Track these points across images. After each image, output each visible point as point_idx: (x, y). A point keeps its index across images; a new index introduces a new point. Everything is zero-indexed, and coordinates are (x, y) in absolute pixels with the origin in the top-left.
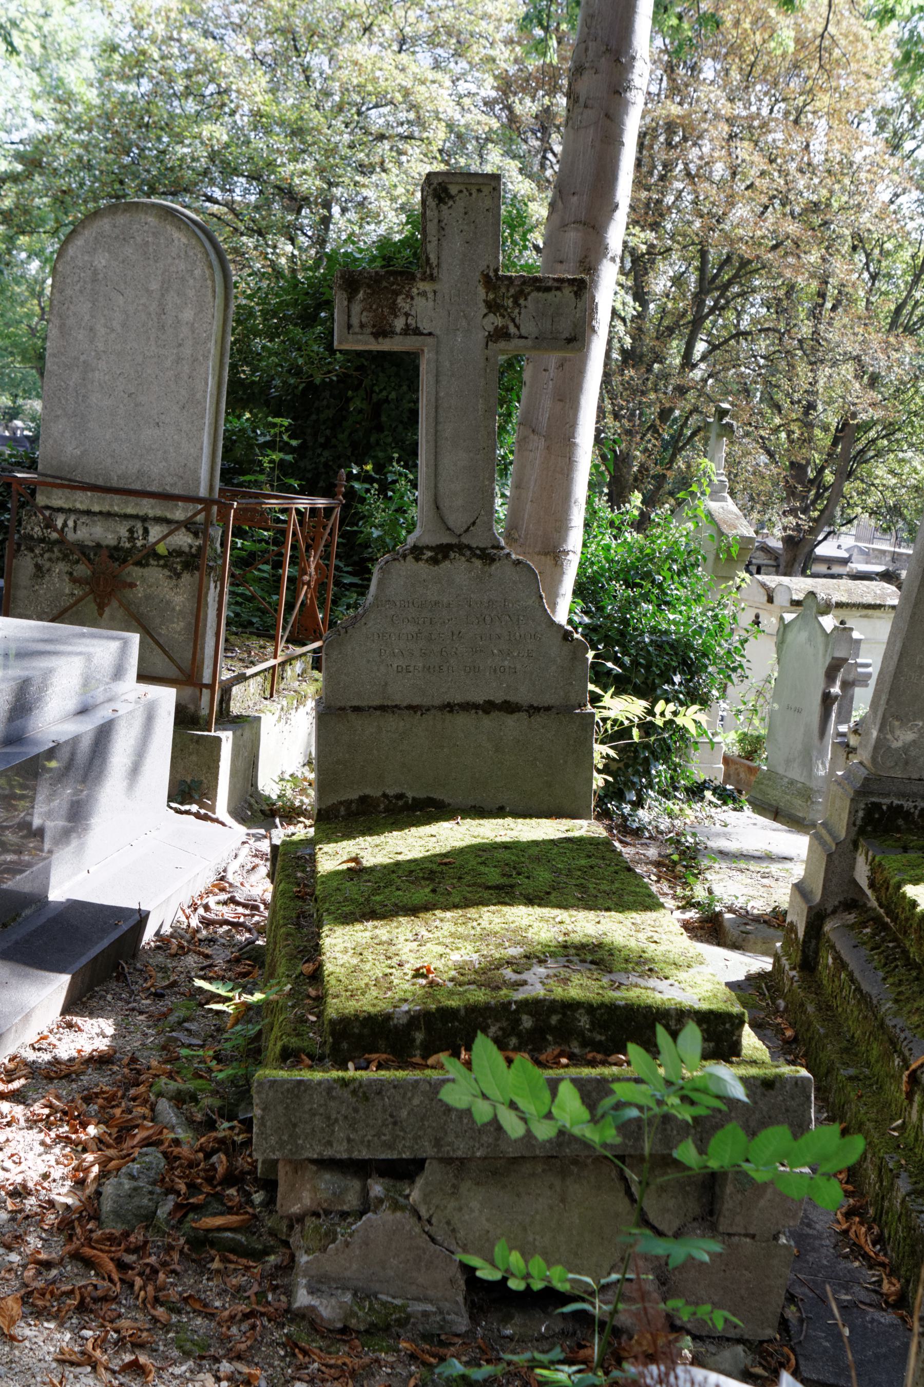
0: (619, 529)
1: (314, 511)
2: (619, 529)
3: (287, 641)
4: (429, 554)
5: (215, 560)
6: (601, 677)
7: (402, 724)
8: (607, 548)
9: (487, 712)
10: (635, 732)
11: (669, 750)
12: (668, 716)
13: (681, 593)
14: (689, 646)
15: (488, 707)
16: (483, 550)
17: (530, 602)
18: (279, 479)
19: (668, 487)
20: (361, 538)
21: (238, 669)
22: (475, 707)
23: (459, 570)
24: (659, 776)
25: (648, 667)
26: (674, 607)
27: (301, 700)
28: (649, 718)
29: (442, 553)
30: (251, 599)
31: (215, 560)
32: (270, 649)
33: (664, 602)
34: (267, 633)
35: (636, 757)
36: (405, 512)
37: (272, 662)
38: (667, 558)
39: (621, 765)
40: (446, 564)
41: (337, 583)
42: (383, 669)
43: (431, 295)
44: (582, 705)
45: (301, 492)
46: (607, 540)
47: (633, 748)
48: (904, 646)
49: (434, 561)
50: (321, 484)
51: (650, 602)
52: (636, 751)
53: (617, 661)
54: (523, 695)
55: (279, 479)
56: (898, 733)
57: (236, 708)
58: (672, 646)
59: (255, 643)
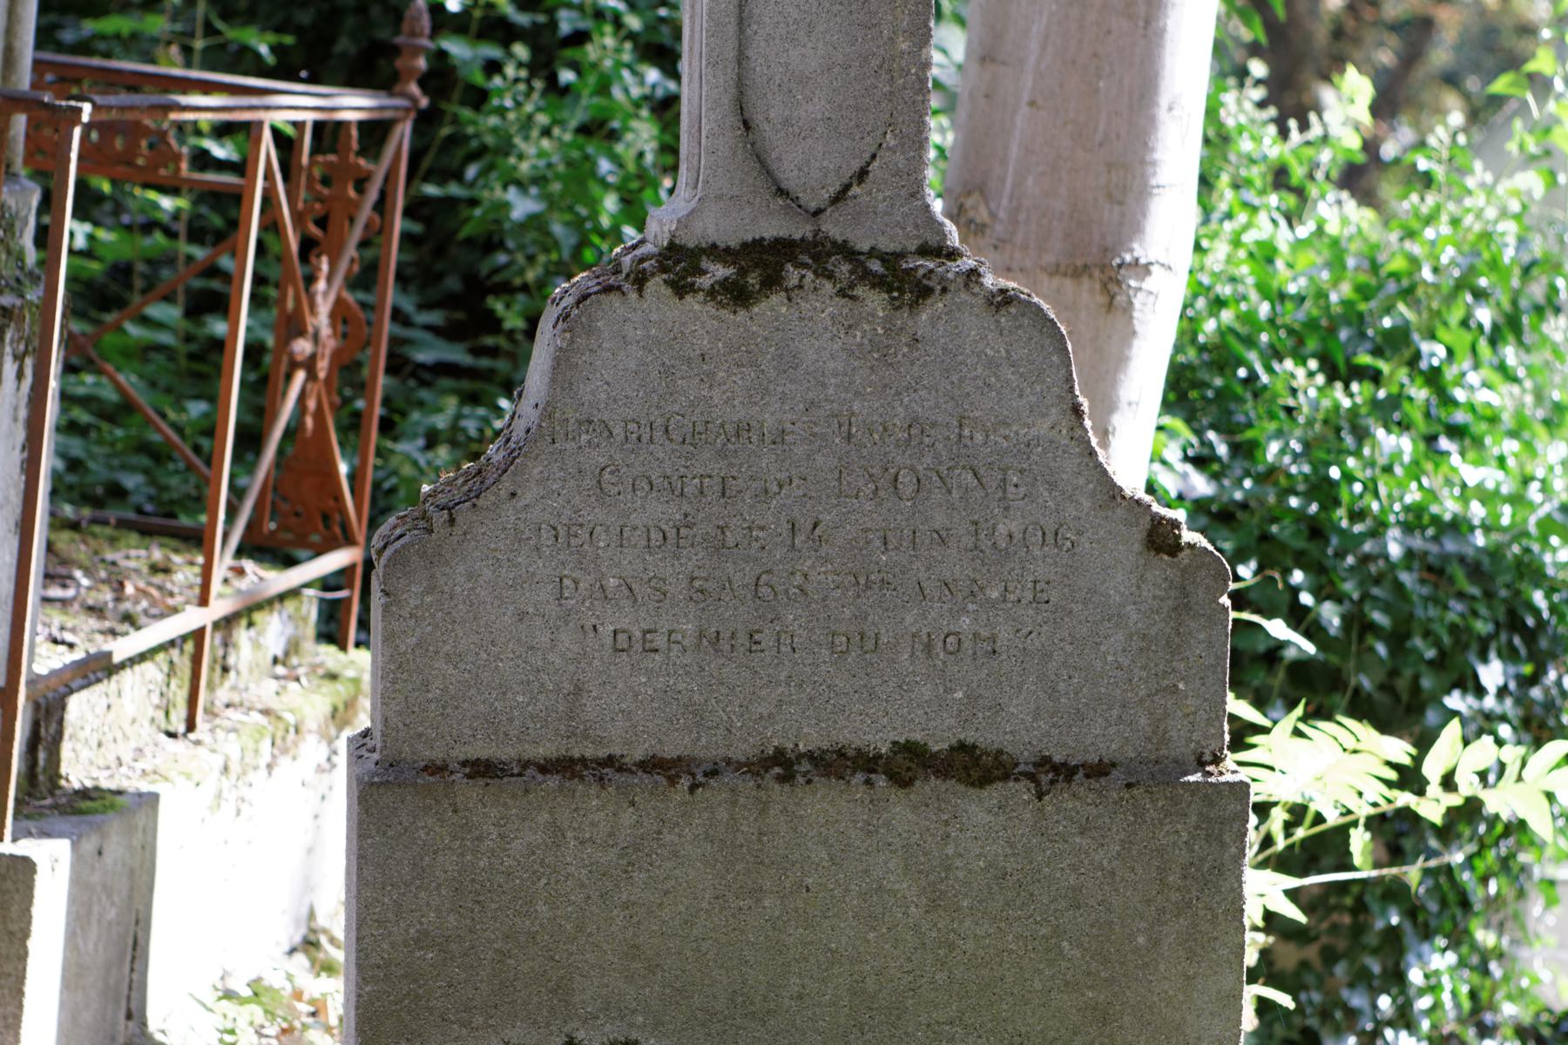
0: (1300, 192)
1: (327, 133)
2: (1300, 192)
3: (239, 553)
4: (719, 271)
5: (17, 288)
6: (1257, 669)
7: (628, 817)
8: (1265, 255)
9: (902, 781)
10: (1359, 841)
11: (1465, 904)
12: (1468, 785)
13: (1499, 398)
14: (1529, 570)
15: (907, 765)
16: (891, 259)
17: (1042, 428)
18: (210, 30)
19: (1440, 56)
20: (473, 223)
21: (87, 639)
22: (867, 763)
23: (812, 323)
24: (1433, 988)
25: (1398, 639)
26: (1478, 443)
27: (285, 736)
28: (1404, 799)
29: (759, 268)
30: (125, 408)
31: (17, 288)
32: (185, 574)
33: (1450, 429)
34: (175, 523)
35: (1358, 930)
36: (614, 136)
37: (192, 618)
38: (1462, 285)
39: (1311, 952)
40: (773, 306)
41: (396, 365)
42: (567, 639)
44: (1207, 760)
45: (285, 69)
46: (1262, 229)
47: (1358, 899)
49: (736, 295)
50: (344, 45)
51: (1404, 426)
52: (1360, 908)
53: (1298, 617)
54: (1017, 728)
55: (210, 30)
57: (78, 766)
58: (1475, 570)
59: (135, 556)
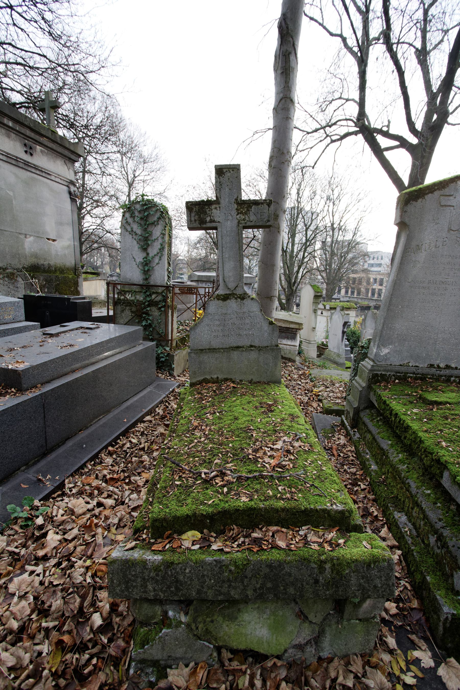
23: (233, 304)
43: (218, 209)
48: (385, 321)
56: (383, 350)
